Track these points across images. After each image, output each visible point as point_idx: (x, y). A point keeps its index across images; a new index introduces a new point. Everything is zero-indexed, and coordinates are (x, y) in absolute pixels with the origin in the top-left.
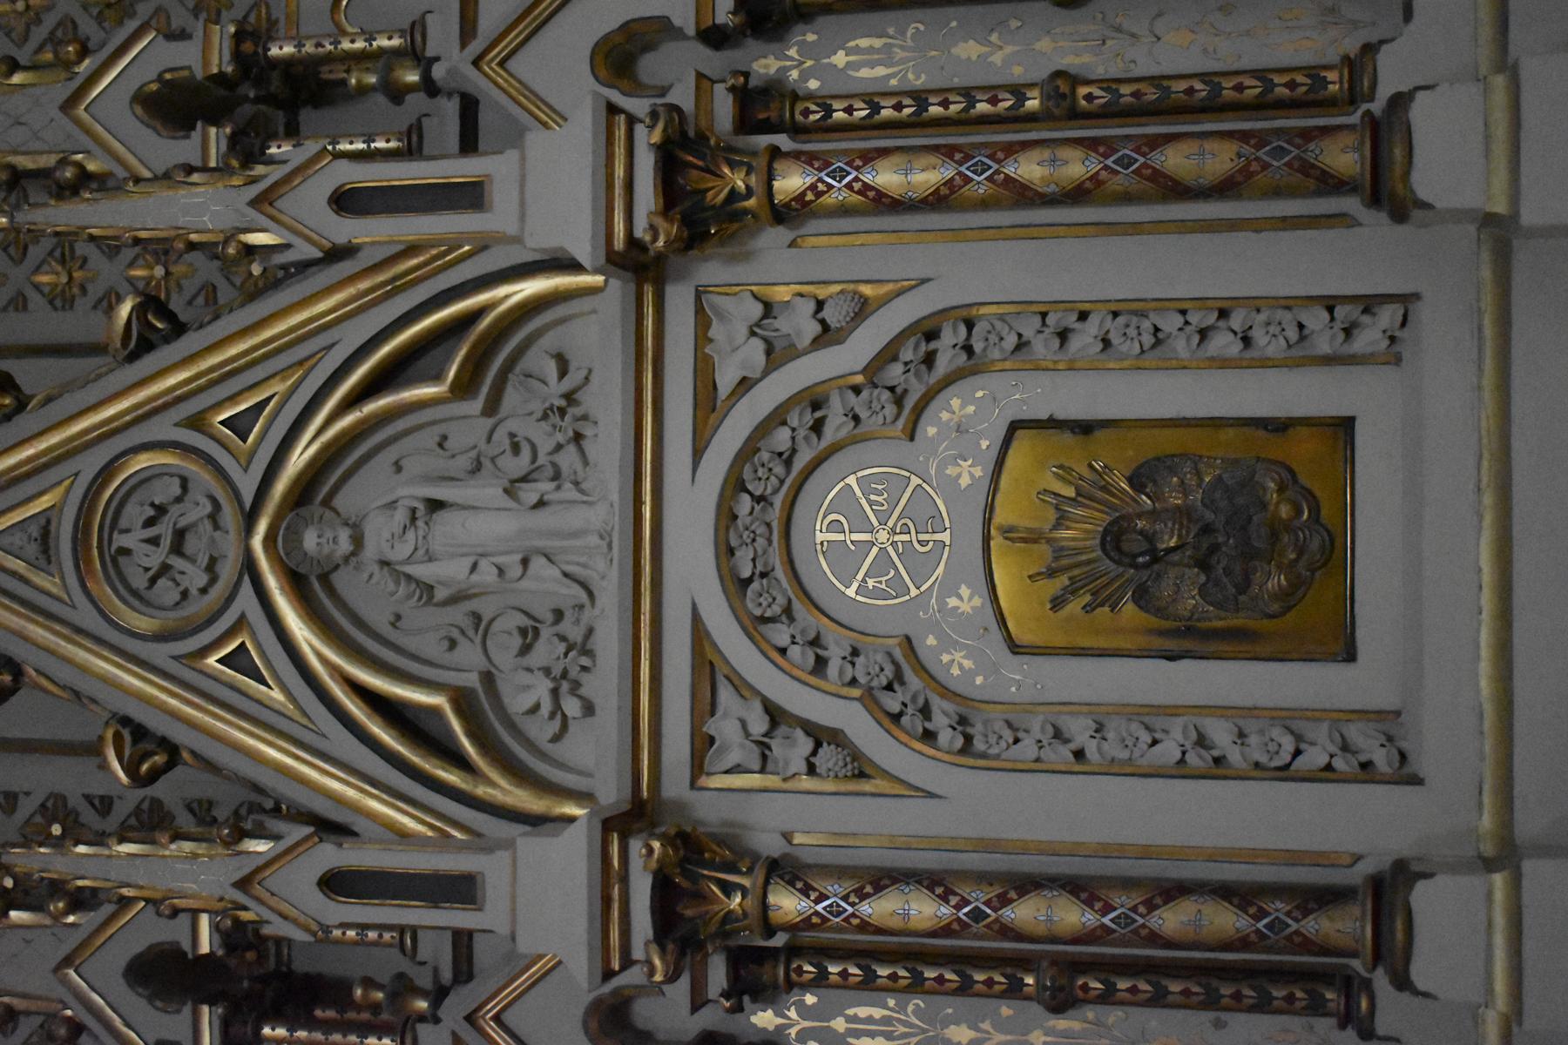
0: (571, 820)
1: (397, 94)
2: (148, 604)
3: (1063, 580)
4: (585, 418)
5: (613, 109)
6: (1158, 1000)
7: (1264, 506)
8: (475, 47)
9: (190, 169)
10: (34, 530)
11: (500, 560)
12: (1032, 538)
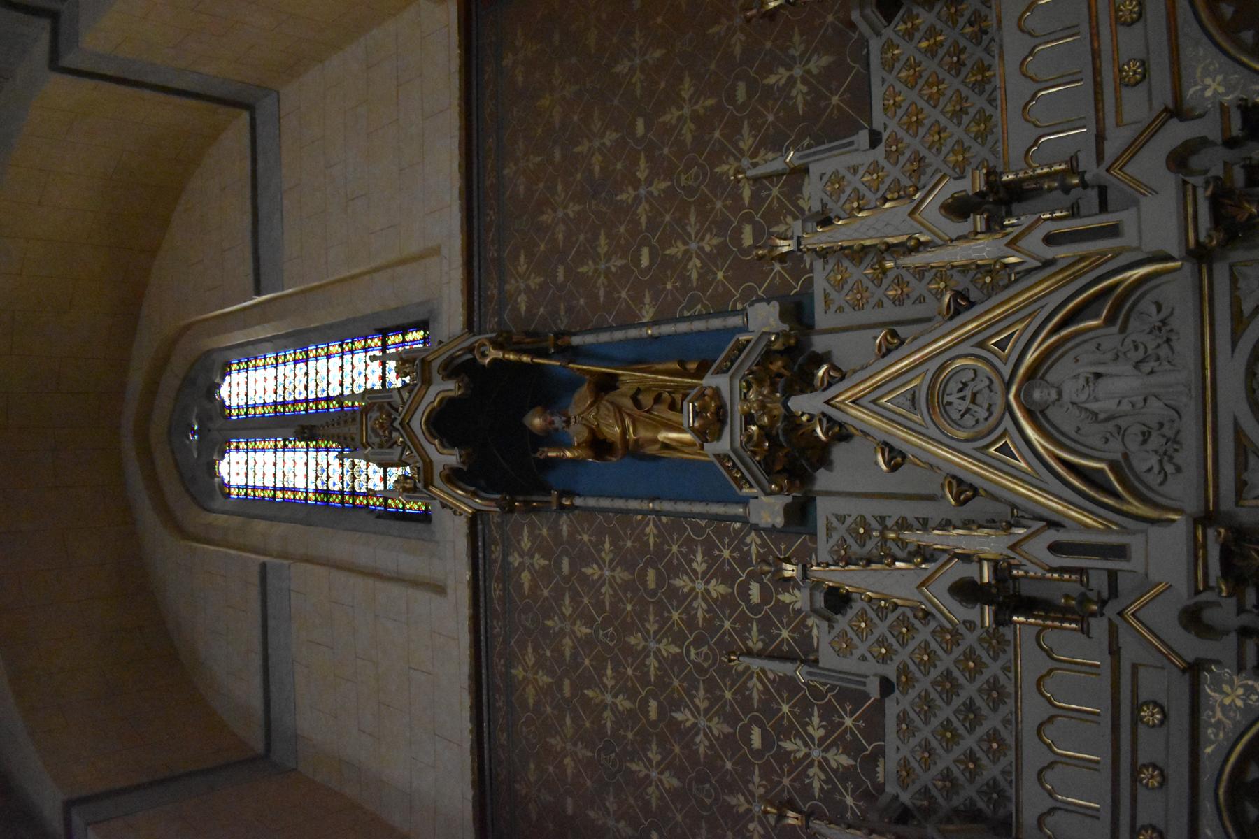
0: (1173, 521)
1: (1066, 189)
4: (1171, 330)
8: (1106, 165)
10: (909, 396)
11: (1134, 399)
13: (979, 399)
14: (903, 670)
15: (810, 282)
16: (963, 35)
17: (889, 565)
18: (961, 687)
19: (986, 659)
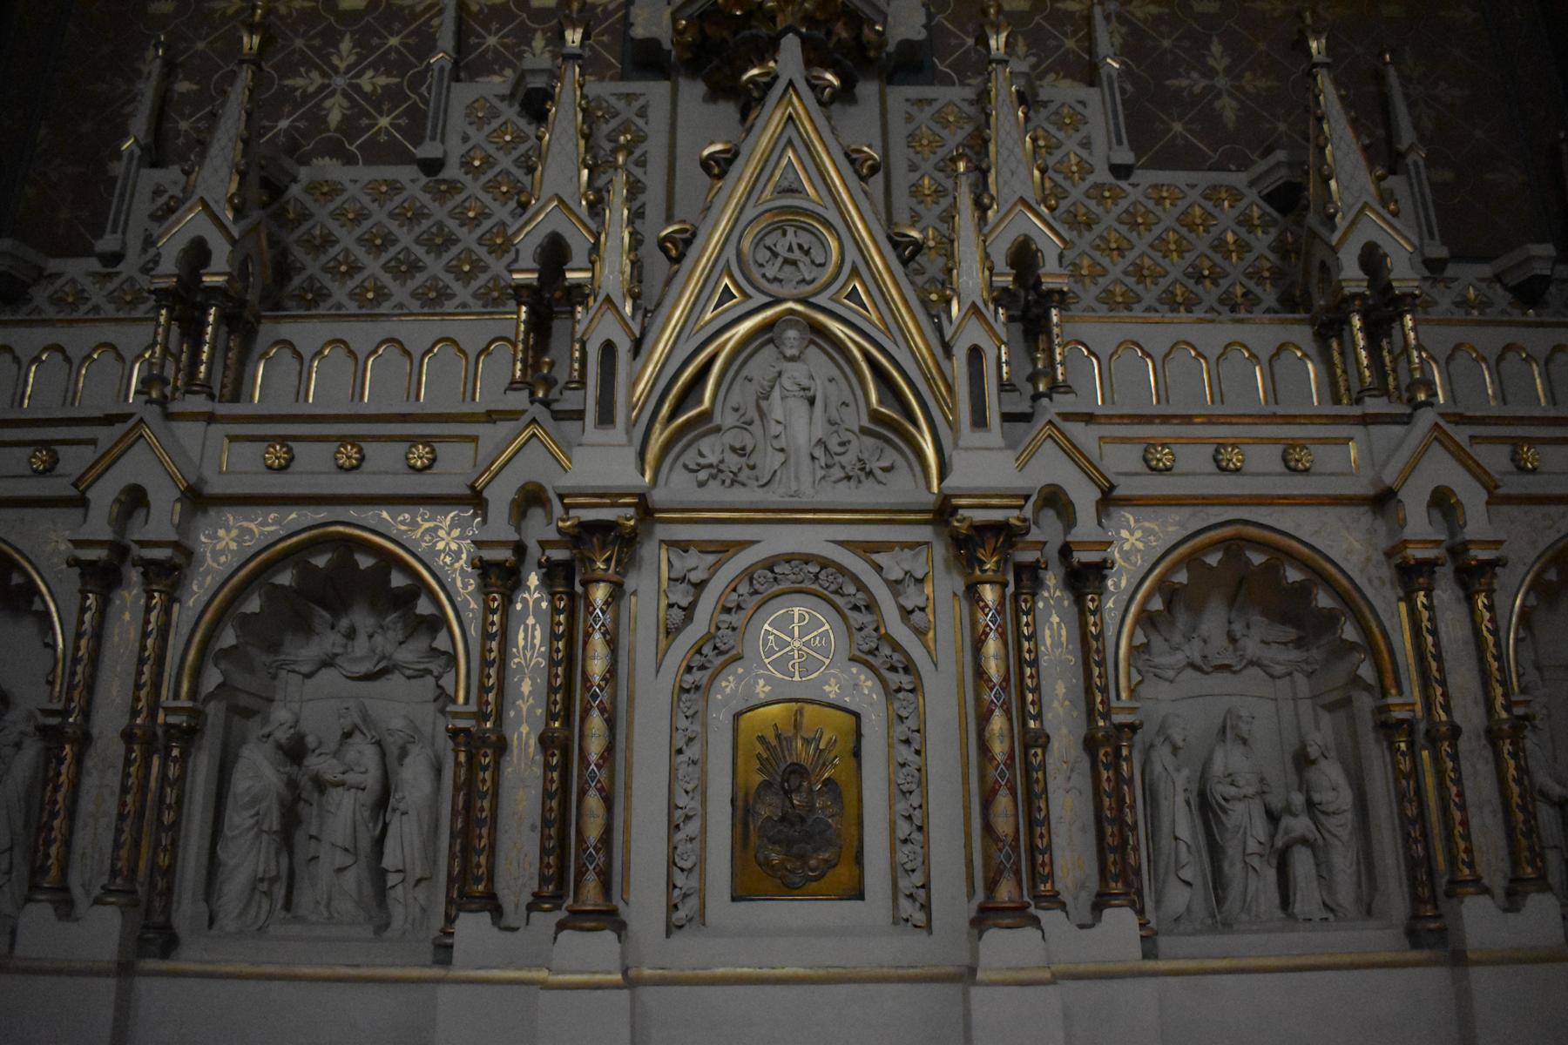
0: (643, 475)
1: (1033, 378)
2: (757, 245)
3: (774, 742)
4: (860, 482)
5: (1027, 498)
6: (547, 795)
7: (816, 850)
8: (1057, 420)
9: (991, 270)
10: (795, 186)
12: (797, 726)
13: (788, 269)
14: (454, 187)
15: (946, 81)
16: (1233, 284)
17: (584, 160)
18: (439, 255)
19: (475, 285)
